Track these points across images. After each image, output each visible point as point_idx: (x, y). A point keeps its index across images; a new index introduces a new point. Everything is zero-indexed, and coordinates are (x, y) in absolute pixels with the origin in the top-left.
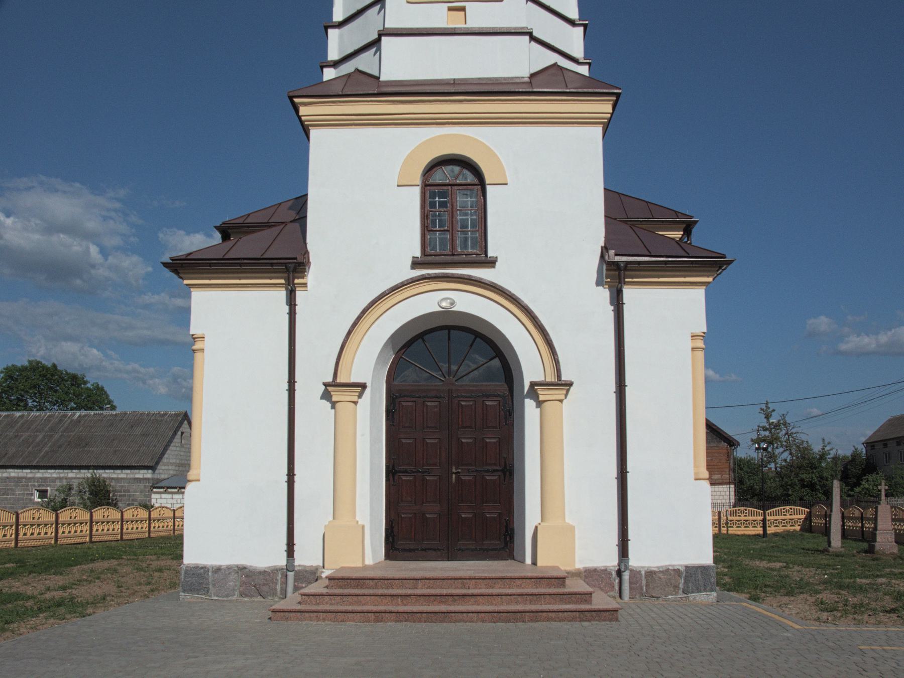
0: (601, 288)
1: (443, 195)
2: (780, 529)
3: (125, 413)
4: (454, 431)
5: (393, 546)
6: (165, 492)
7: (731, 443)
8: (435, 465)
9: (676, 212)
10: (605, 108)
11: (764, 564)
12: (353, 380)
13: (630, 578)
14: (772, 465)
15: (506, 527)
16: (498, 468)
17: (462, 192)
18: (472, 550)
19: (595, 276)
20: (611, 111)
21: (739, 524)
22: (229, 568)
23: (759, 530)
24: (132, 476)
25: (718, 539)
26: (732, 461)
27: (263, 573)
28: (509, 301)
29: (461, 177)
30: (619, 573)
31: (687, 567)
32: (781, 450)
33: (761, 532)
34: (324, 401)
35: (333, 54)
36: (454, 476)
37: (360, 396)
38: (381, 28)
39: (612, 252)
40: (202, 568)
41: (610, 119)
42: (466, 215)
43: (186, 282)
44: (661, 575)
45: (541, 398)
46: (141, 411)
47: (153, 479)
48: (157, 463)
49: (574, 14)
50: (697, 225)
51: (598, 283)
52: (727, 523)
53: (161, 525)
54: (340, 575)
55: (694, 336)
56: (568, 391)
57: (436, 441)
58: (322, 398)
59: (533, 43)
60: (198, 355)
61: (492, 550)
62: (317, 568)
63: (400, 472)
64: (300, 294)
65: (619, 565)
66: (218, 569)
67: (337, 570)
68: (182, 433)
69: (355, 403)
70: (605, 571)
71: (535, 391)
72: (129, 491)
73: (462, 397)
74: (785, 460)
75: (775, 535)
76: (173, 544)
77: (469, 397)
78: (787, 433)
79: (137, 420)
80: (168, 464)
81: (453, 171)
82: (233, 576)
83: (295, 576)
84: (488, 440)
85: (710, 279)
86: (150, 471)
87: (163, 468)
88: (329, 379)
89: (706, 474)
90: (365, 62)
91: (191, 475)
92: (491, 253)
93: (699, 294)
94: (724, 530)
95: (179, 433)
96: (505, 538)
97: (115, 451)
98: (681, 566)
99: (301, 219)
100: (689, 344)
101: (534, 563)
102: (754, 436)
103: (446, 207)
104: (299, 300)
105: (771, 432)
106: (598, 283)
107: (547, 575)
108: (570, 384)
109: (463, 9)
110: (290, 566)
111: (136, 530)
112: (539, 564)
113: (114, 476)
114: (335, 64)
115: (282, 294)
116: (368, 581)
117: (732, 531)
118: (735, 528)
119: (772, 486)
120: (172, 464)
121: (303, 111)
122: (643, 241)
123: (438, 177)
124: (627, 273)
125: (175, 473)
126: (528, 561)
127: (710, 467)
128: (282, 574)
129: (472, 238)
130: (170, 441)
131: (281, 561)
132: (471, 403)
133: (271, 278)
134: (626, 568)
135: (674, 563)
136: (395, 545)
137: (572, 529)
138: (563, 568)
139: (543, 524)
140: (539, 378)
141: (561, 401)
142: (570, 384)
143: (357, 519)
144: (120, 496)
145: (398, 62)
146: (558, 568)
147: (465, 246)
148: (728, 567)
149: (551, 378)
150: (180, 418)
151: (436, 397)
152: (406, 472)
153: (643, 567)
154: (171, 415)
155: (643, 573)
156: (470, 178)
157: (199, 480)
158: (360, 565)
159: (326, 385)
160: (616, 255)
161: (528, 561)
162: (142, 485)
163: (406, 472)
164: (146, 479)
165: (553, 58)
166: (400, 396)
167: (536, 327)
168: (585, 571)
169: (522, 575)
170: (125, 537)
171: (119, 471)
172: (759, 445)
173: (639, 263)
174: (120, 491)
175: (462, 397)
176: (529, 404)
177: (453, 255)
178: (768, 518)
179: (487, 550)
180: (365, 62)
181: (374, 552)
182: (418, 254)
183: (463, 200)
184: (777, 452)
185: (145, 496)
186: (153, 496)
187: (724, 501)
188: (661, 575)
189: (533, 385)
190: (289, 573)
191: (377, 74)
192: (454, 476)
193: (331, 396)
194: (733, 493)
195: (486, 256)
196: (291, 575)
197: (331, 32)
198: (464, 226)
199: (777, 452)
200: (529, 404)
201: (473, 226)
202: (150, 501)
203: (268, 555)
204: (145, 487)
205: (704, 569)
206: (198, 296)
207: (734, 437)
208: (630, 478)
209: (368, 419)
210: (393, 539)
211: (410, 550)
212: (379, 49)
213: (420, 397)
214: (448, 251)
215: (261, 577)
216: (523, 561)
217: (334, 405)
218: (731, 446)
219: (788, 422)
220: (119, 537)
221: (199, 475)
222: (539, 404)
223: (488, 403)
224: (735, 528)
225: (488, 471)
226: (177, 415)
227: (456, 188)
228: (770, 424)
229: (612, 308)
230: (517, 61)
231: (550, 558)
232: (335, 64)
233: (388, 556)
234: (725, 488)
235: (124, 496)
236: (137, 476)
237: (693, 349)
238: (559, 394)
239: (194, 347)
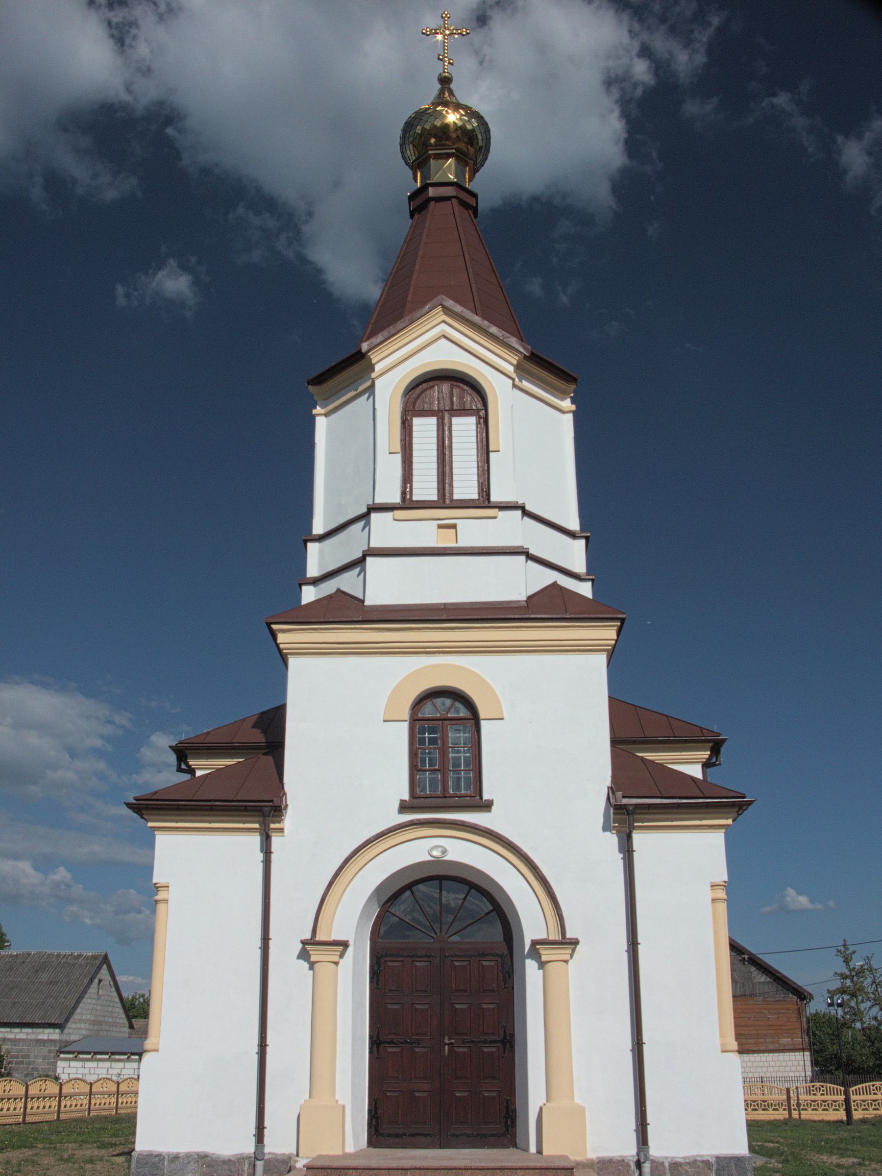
0: (608, 833)
1: (432, 730)
2: (870, 1114)
3: (29, 954)
4: (446, 996)
5: (376, 1130)
6: (76, 1059)
7: (802, 995)
8: (425, 1034)
9: (701, 728)
10: (608, 633)
11: (835, 1159)
12: (334, 937)
13: (651, 1168)
14: (858, 1025)
15: (507, 1108)
16: (497, 1038)
17: (455, 727)
18: (469, 1136)
19: (601, 820)
20: (615, 637)
21: (815, 1105)
22: (188, 1156)
23: (842, 1115)
24: (33, 1037)
25: (752, 1126)
26: (804, 1020)
27: (228, 1162)
28: (507, 849)
29: (452, 710)
30: (639, 1165)
31: (718, 1158)
32: (869, 1004)
33: (845, 1118)
34: (301, 961)
35: (312, 571)
36: (447, 1047)
37: (341, 956)
38: (366, 548)
39: (619, 794)
40: (157, 1156)
41: (614, 646)
42: (459, 752)
43: (150, 824)
44: (687, 1168)
45: (544, 958)
46: (49, 952)
47: (60, 1041)
48: (67, 1020)
49: (574, 525)
50: (726, 743)
51: (605, 828)
52: (798, 1105)
53: (74, 1103)
54: (319, 1163)
55: (713, 886)
56: (573, 951)
57: (426, 1007)
58: (299, 957)
59: (529, 562)
60: (161, 907)
61: (491, 1135)
62: (290, 1157)
63: (385, 1042)
64: (276, 841)
65: (638, 1154)
66: (175, 1158)
67: (314, 1159)
68: (100, 981)
69: (336, 963)
70: (622, 1163)
71: (537, 951)
72: (28, 1057)
73: (456, 956)
74: (876, 1018)
75: (864, 1121)
76: (124, 1125)
77: (462, 956)
78: (874, 982)
79: (42, 964)
80: (80, 1021)
81: (444, 704)
82: (192, 1166)
83: (265, 1165)
84: (485, 1006)
85: (730, 822)
86: (57, 1031)
87: (74, 1026)
88: (308, 936)
89: (734, 1045)
90: (348, 583)
91: (149, 1044)
92: (486, 797)
93: (719, 838)
94: (795, 1114)
95: (96, 981)
96: (506, 1122)
97: (14, 1003)
98: (711, 1156)
99: (274, 747)
100: (709, 894)
101: (540, 1151)
102: (836, 984)
103: (437, 744)
104: (274, 848)
105: (852, 981)
106: (605, 828)
107: (552, 1165)
108: (575, 943)
109: (454, 527)
110: (259, 1154)
111: (43, 1110)
112: (545, 1153)
113: (11, 1036)
114: (315, 582)
115: (255, 840)
116: (351, 1171)
117: (805, 1115)
118: (810, 1111)
119: (864, 1056)
120: (86, 1021)
121: (281, 638)
122: (638, 801)
123: (428, 711)
124: (636, 817)
125: (88, 1033)
126: (533, 1149)
127: (738, 1036)
128: (249, 1164)
129: (465, 778)
130: (85, 992)
131: (249, 1148)
132: (466, 963)
133: (244, 822)
134: (647, 1158)
135: (703, 1153)
136: (381, 1130)
137: (582, 1110)
138: (572, 1158)
139: (548, 1104)
140: (542, 935)
141: (566, 962)
142: (575, 943)
143: (337, 1097)
144: (17, 1063)
145: (383, 585)
146: (567, 1157)
147: (457, 787)
148: (782, 1163)
149: (555, 936)
150: (98, 962)
151: (426, 956)
152: (392, 1042)
153: (666, 1158)
154: (87, 958)
155: (667, 1164)
156: (463, 712)
157: (157, 1050)
158: (339, 1152)
159: (304, 943)
160: (624, 797)
161: (533, 1149)
162: (45, 1050)
163: (392, 1042)
164: (51, 1041)
165: (550, 577)
166: (386, 956)
167: (536, 878)
168: (599, 1162)
169: (525, 1164)
170: (29, 1119)
171: (17, 1030)
172: (832, 998)
173: (649, 805)
174: (17, 1057)
175: (456, 956)
176: (531, 965)
177: (445, 797)
178: (853, 1097)
179: (485, 1136)
180: (348, 583)
181: (356, 1137)
182: (406, 797)
183: (456, 736)
184: (863, 1006)
185: (48, 1064)
186: (60, 1064)
187: (797, 1074)
188: (687, 1168)
189: (535, 943)
190: (258, 1163)
191: (361, 597)
192: (447, 1047)
193: (310, 956)
194: (808, 1063)
195: (481, 798)
196: (260, 1164)
197: (310, 545)
198: (457, 764)
199: (863, 1006)
200: (531, 965)
201: (467, 764)
202: (55, 1070)
203: (233, 1141)
204: (50, 1051)
205: (738, 1160)
206: (161, 839)
207: (806, 988)
208: (646, 1049)
209: (350, 983)
210: (377, 1122)
211: (397, 1136)
212: (363, 570)
213: (408, 956)
214: (439, 792)
215: (226, 1167)
216: (526, 1149)
217: (312, 965)
218: (804, 999)
219: (874, 967)
220: (21, 1120)
221: (158, 1044)
222: (542, 965)
223: (484, 963)
224: (810, 1111)
225: (485, 1042)
226: (94, 957)
227: (447, 722)
228: (850, 970)
229: (621, 856)
230: (516, 582)
231: (557, 1145)
232: (315, 582)
233: (371, 1143)
234: (798, 1055)
235: (22, 1063)
236: (40, 1037)
237: (714, 900)
238: (563, 953)
239: (157, 898)
